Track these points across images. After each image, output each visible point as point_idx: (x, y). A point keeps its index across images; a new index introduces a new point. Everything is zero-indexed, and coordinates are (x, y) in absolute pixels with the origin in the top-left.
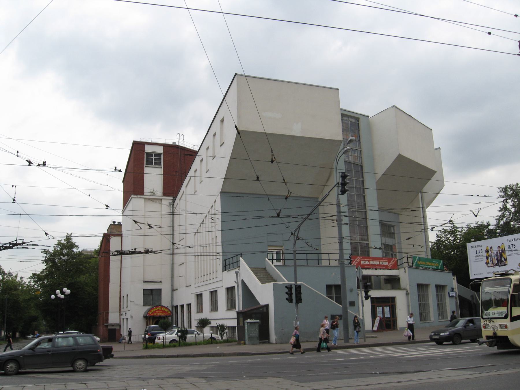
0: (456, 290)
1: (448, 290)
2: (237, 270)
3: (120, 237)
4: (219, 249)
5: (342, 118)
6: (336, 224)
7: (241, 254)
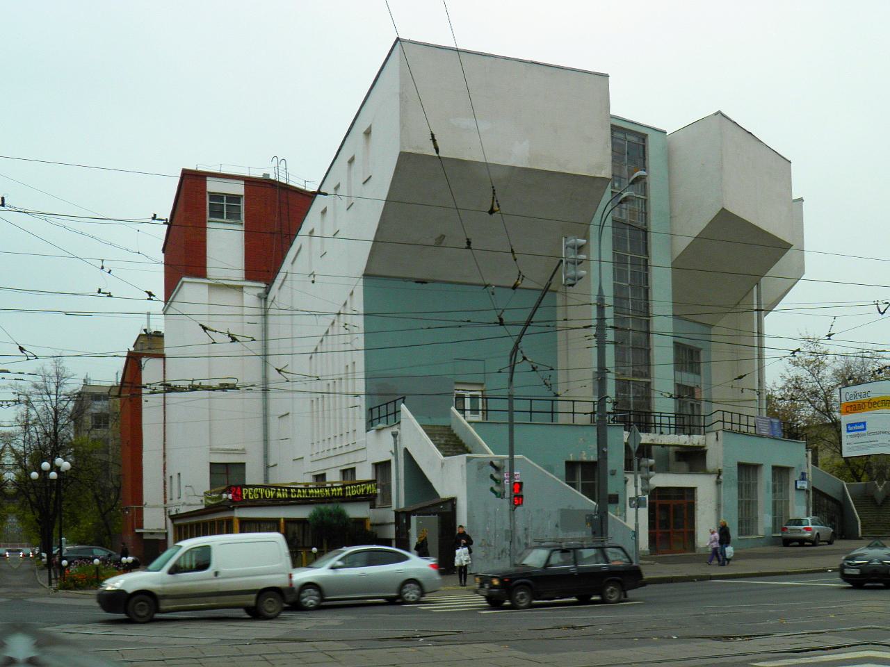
0: (810, 476)
1: (795, 476)
2: (395, 429)
3: (160, 361)
4: (360, 387)
5: (612, 134)
6: (594, 342)
7: (404, 398)
